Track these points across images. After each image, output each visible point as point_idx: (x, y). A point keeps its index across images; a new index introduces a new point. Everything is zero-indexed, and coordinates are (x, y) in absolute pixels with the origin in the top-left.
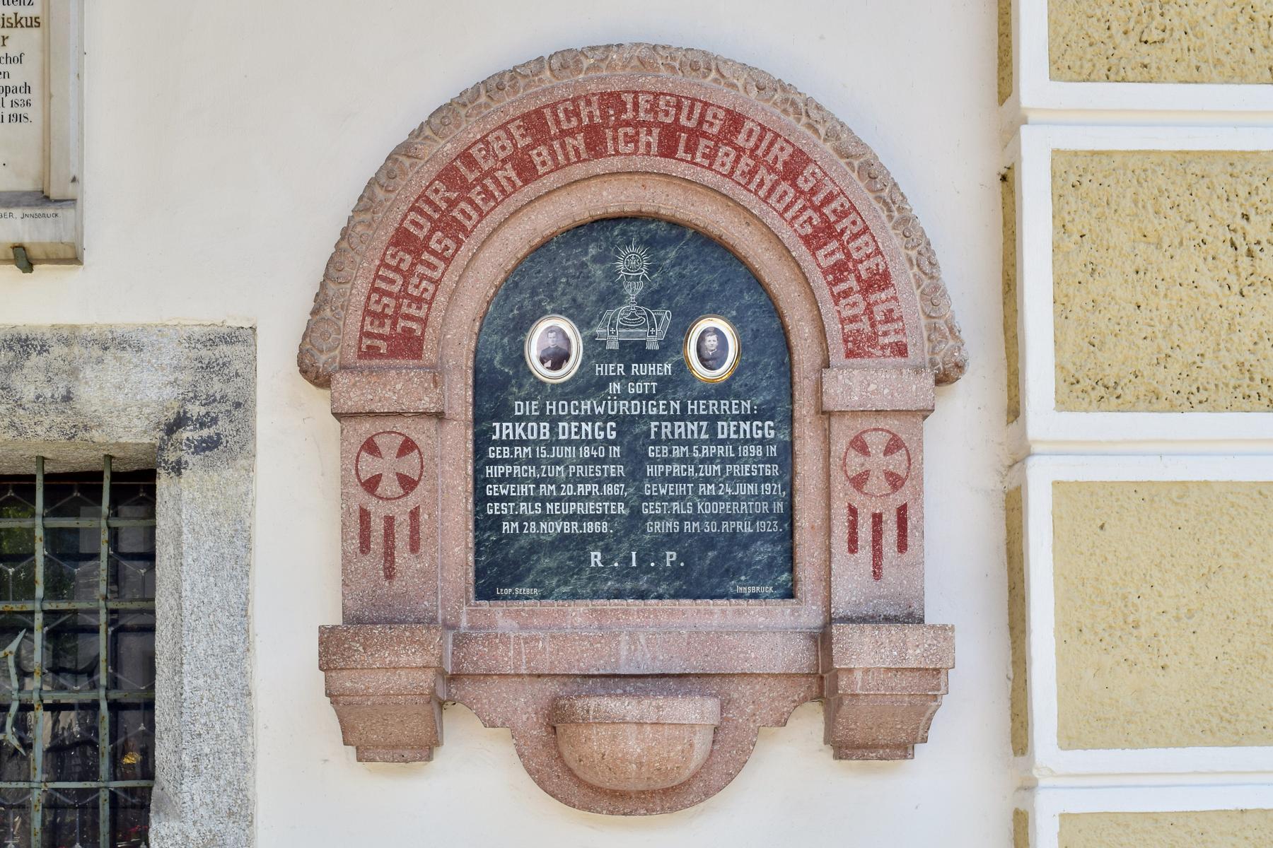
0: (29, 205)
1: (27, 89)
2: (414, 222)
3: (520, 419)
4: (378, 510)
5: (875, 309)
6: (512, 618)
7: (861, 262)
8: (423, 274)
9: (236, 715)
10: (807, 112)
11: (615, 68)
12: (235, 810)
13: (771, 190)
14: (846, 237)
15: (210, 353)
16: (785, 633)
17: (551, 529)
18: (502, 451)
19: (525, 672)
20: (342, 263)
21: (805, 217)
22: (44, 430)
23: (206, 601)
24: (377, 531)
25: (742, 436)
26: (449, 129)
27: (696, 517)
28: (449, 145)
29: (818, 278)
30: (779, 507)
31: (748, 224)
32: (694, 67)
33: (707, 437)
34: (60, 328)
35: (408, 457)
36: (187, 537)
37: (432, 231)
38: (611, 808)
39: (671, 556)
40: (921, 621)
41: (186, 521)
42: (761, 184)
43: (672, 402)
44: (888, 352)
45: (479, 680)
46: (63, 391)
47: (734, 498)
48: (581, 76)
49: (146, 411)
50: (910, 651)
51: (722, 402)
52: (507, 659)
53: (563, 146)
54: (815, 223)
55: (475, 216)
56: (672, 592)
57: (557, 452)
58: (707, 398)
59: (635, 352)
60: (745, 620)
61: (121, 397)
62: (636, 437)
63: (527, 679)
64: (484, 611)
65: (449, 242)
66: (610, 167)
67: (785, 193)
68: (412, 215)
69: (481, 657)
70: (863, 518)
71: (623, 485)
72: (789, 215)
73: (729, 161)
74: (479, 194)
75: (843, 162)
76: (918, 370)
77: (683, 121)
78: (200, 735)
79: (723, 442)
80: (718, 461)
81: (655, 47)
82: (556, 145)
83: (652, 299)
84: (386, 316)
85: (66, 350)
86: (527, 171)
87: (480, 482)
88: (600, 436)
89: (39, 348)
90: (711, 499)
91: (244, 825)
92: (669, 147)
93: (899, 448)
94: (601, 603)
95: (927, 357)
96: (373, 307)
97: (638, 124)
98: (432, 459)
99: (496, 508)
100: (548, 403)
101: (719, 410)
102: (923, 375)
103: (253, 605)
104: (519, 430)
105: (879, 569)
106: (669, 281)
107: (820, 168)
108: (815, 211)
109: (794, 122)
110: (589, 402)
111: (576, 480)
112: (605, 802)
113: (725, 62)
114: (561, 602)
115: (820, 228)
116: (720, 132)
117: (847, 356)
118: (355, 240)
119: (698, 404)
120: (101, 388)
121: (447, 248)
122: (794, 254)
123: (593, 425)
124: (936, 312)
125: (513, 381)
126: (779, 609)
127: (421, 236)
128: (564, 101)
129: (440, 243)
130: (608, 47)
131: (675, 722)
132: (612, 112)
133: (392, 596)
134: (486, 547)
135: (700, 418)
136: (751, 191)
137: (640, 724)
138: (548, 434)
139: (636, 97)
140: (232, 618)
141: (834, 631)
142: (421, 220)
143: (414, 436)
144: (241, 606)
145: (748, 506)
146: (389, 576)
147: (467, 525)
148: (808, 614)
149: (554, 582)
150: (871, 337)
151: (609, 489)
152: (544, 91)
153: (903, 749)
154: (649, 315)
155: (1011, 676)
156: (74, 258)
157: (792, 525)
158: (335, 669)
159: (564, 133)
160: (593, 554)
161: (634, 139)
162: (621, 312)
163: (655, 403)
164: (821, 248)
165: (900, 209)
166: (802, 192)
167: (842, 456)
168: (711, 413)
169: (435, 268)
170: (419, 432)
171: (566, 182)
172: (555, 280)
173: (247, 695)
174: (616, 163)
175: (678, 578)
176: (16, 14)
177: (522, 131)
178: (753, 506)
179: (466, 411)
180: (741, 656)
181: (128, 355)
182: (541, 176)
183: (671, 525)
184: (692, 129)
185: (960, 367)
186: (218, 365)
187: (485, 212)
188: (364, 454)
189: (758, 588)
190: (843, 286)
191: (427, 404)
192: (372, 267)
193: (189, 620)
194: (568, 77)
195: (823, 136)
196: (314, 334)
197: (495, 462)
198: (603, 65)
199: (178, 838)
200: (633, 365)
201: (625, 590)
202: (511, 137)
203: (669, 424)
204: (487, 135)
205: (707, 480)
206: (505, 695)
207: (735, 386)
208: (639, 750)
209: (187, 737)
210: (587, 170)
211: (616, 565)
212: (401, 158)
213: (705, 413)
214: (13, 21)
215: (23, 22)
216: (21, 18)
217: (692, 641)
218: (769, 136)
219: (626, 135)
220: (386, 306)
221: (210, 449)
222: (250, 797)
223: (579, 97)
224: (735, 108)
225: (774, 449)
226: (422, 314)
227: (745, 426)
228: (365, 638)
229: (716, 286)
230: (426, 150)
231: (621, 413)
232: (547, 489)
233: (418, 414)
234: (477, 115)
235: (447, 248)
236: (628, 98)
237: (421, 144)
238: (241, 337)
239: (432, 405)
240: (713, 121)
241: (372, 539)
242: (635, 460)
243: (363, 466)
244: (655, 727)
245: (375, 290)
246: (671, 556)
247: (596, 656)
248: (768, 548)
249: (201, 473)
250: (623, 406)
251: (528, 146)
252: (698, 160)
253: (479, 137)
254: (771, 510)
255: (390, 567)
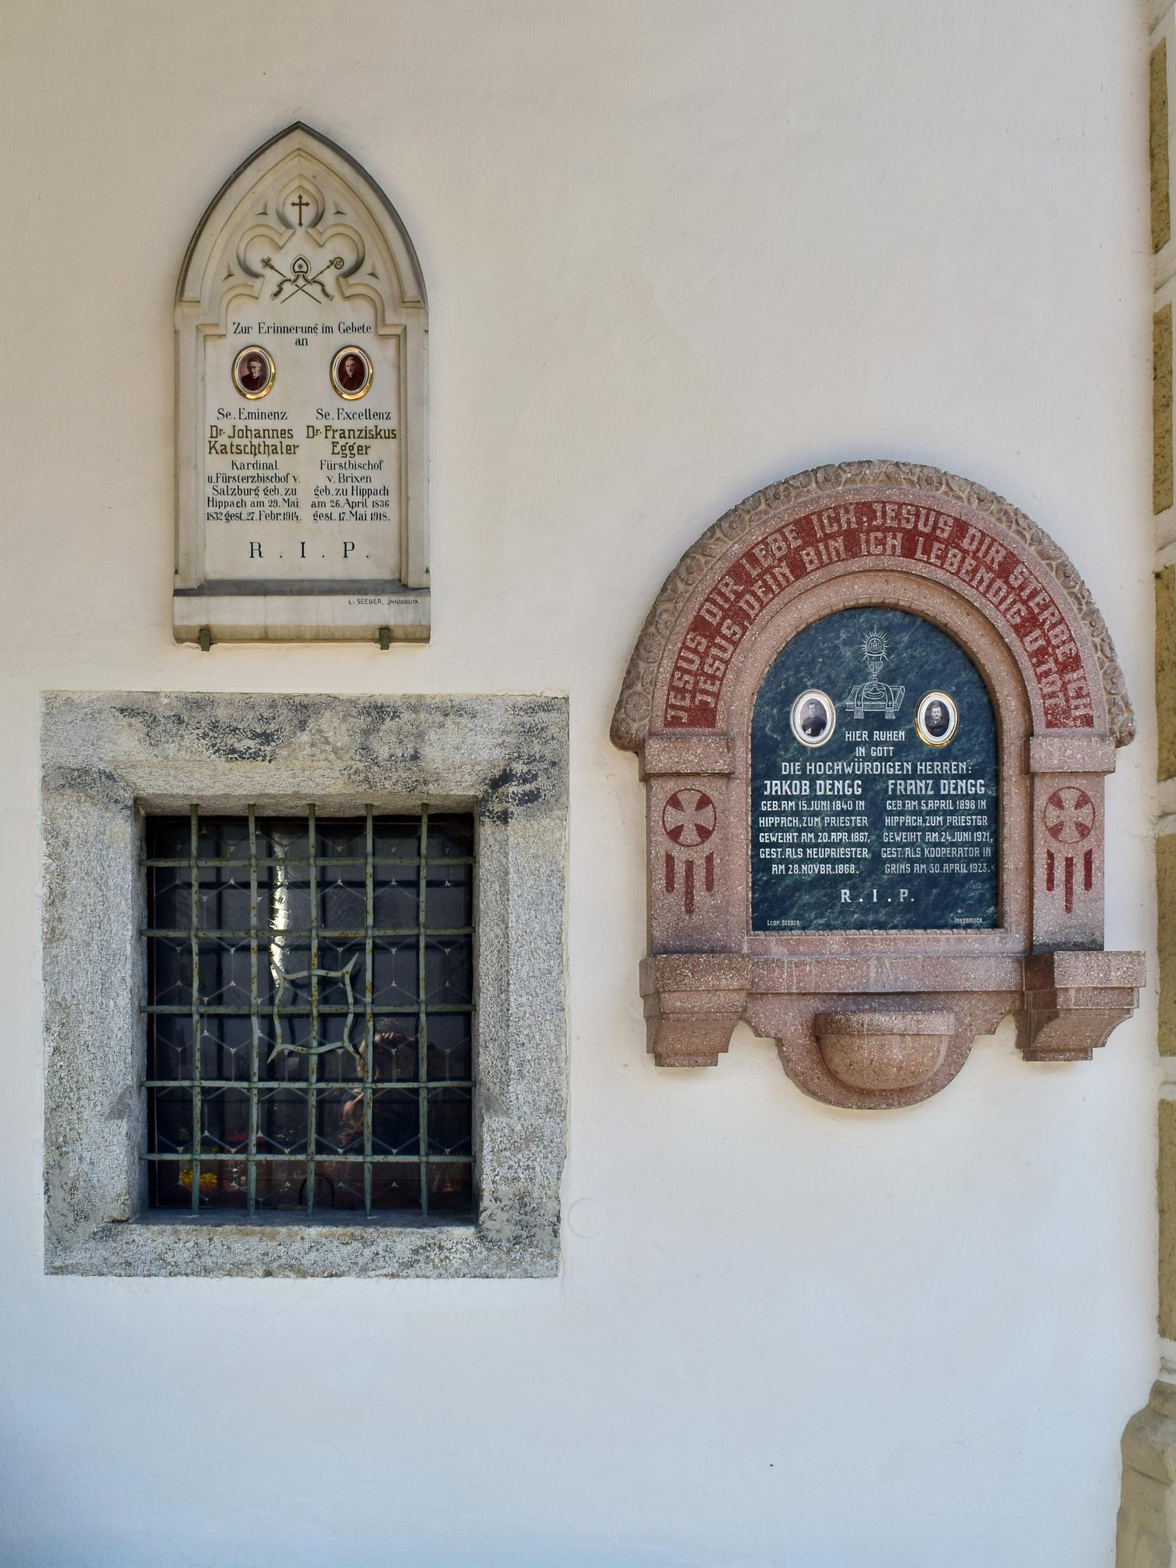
0: (393, 593)
1: (386, 491)
2: (708, 611)
3: (786, 778)
4: (681, 856)
5: (1069, 686)
6: (783, 946)
7: (1058, 647)
8: (716, 655)
9: (552, 1028)
10: (1017, 521)
11: (867, 482)
12: (551, 1107)
13: (989, 586)
14: (1046, 627)
15: (531, 719)
16: (998, 958)
17: (810, 870)
18: (772, 804)
19: (795, 991)
20: (651, 645)
21: (1014, 610)
22: (391, 784)
23: (528, 930)
24: (679, 873)
25: (959, 792)
26: (736, 532)
27: (924, 860)
28: (736, 546)
29: (1025, 660)
30: (988, 851)
31: (968, 614)
32: (929, 481)
33: (932, 793)
34: (410, 697)
35: (705, 810)
36: (513, 876)
37: (723, 619)
38: (859, 1104)
39: (904, 893)
40: (1100, 948)
41: (512, 863)
42: (981, 581)
43: (905, 764)
44: (1078, 723)
45: (757, 998)
46: (411, 751)
47: (952, 844)
48: (840, 488)
49: (478, 768)
50: (1113, 973)
51: (944, 763)
52: (783, 980)
53: (827, 547)
54: (1023, 614)
55: (757, 605)
56: (904, 923)
57: (816, 806)
58: (933, 760)
59: (876, 721)
60: (965, 946)
61: (458, 757)
62: (877, 793)
63: (794, 997)
64: (760, 939)
65: (736, 628)
66: (864, 566)
67: (1000, 589)
68: (708, 605)
69: (762, 979)
70: (1058, 862)
71: (866, 834)
72: (1003, 607)
73: (956, 561)
74: (760, 587)
75: (1044, 562)
76: (1103, 738)
77: (921, 527)
78: (523, 1044)
79: (944, 797)
80: (941, 813)
81: (897, 464)
82: (821, 547)
83: (889, 676)
84: (687, 691)
85: (414, 716)
86: (799, 569)
87: (756, 830)
88: (848, 792)
89: (392, 714)
90: (936, 845)
91: (558, 1120)
92: (909, 550)
93: (1086, 803)
94: (852, 933)
95: (1108, 727)
96: (676, 683)
97: (885, 530)
98: (723, 812)
99: (767, 853)
100: (808, 764)
101: (942, 770)
102: (1108, 742)
103: (567, 935)
104: (785, 787)
105: (1071, 903)
106: (903, 661)
107: (1027, 568)
108: (1023, 605)
109: (1006, 529)
110: (840, 764)
111: (830, 829)
112: (855, 1099)
113: (953, 477)
114: (821, 932)
115: (1026, 619)
116: (949, 537)
117: (1047, 727)
118: (661, 626)
119: (926, 764)
120: (443, 749)
121: (735, 633)
122: (1006, 640)
123: (844, 783)
124: (1115, 689)
125: (781, 745)
126: (991, 937)
127: (715, 623)
128: (828, 509)
129: (730, 629)
130: (860, 463)
131: (931, 1033)
132: (865, 519)
133: (692, 928)
134: (759, 885)
135: (927, 777)
136: (973, 587)
137: (903, 1035)
138: (808, 790)
139: (884, 507)
140: (549, 945)
141: (1056, 957)
142: (714, 609)
143: (709, 793)
144: (556, 935)
145: (964, 851)
146: (690, 911)
147: (748, 868)
148: (1012, 941)
149: (813, 915)
150: (1066, 710)
151: (857, 837)
152: (812, 500)
153: (1084, 1053)
154: (888, 689)
155: (1159, 991)
156: (423, 636)
157: (997, 867)
158: (670, 991)
159: (828, 537)
160: (843, 891)
161: (882, 542)
162: (865, 688)
163: (892, 764)
164: (1027, 635)
165: (1088, 603)
166: (1013, 588)
167: (1043, 810)
168: (936, 773)
169: (725, 650)
170: (713, 790)
171: (829, 578)
172: (813, 661)
173: (561, 1010)
174: (869, 562)
175: (909, 911)
176: (376, 427)
177: (795, 534)
178: (968, 850)
179: (747, 771)
180: (964, 976)
181: (464, 720)
182: (809, 573)
183: (904, 867)
184: (927, 534)
185: (1131, 735)
186: (537, 729)
187: (765, 603)
188: (669, 808)
189: (971, 919)
190: (1044, 668)
191: (721, 766)
192: (675, 649)
193: (514, 947)
194: (830, 489)
195: (1028, 541)
196: (629, 706)
197: (767, 814)
198: (858, 479)
199: (506, 1131)
200: (875, 732)
201: (868, 921)
202: (785, 539)
203: (903, 782)
204: (766, 538)
205: (932, 829)
206: (777, 1010)
207: (955, 751)
208: (901, 1057)
209: (513, 1046)
210: (846, 568)
211: (861, 900)
212: (698, 556)
213: (931, 772)
214: (374, 433)
215: (382, 433)
216: (381, 430)
217: (926, 964)
218: (987, 541)
219: (876, 538)
220: (687, 682)
221: (532, 802)
222: (563, 1096)
223: (840, 506)
224: (961, 516)
225: (984, 803)
226: (715, 689)
227: (838, 784)
228: (693, 965)
229: (939, 665)
230: (717, 549)
231: (866, 773)
232: (807, 837)
233: (713, 775)
234: (759, 519)
235: (735, 633)
236: (878, 507)
237: (715, 545)
238: (556, 706)
239: (726, 767)
240: (944, 527)
241: (676, 880)
242: (876, 812)
243: (668, 818)
244: (914, 1037)
245: (677, 668)
246: (904, 893)
247: (851, 977)
248: (979, 885)
249: (524, 822)
250: (867, 767)
251: (799, 547)
252: (932, 560)
253: (760, 539)
254: (981, 854)
255: (690, 903)
